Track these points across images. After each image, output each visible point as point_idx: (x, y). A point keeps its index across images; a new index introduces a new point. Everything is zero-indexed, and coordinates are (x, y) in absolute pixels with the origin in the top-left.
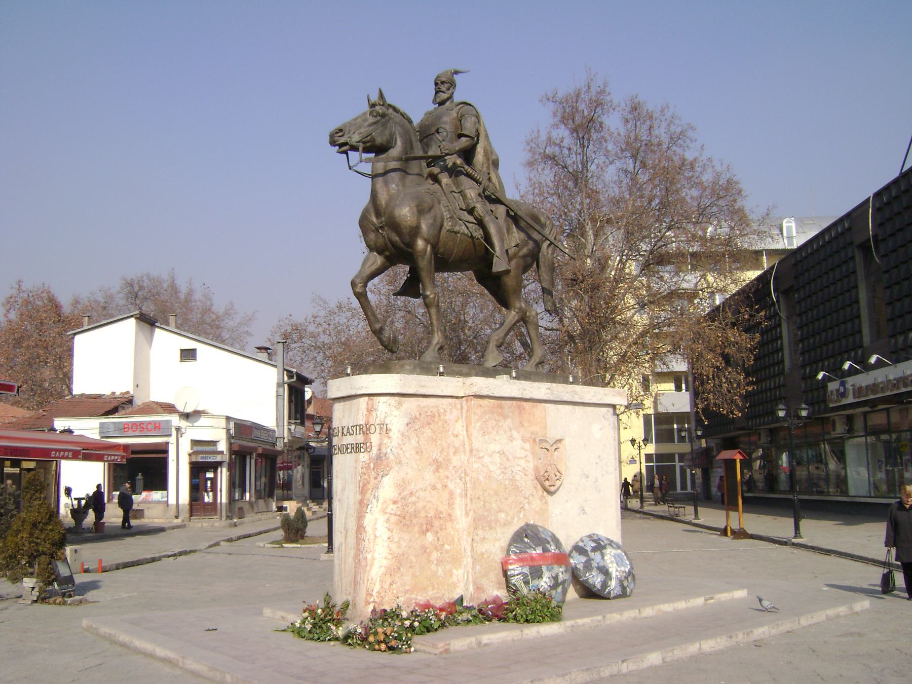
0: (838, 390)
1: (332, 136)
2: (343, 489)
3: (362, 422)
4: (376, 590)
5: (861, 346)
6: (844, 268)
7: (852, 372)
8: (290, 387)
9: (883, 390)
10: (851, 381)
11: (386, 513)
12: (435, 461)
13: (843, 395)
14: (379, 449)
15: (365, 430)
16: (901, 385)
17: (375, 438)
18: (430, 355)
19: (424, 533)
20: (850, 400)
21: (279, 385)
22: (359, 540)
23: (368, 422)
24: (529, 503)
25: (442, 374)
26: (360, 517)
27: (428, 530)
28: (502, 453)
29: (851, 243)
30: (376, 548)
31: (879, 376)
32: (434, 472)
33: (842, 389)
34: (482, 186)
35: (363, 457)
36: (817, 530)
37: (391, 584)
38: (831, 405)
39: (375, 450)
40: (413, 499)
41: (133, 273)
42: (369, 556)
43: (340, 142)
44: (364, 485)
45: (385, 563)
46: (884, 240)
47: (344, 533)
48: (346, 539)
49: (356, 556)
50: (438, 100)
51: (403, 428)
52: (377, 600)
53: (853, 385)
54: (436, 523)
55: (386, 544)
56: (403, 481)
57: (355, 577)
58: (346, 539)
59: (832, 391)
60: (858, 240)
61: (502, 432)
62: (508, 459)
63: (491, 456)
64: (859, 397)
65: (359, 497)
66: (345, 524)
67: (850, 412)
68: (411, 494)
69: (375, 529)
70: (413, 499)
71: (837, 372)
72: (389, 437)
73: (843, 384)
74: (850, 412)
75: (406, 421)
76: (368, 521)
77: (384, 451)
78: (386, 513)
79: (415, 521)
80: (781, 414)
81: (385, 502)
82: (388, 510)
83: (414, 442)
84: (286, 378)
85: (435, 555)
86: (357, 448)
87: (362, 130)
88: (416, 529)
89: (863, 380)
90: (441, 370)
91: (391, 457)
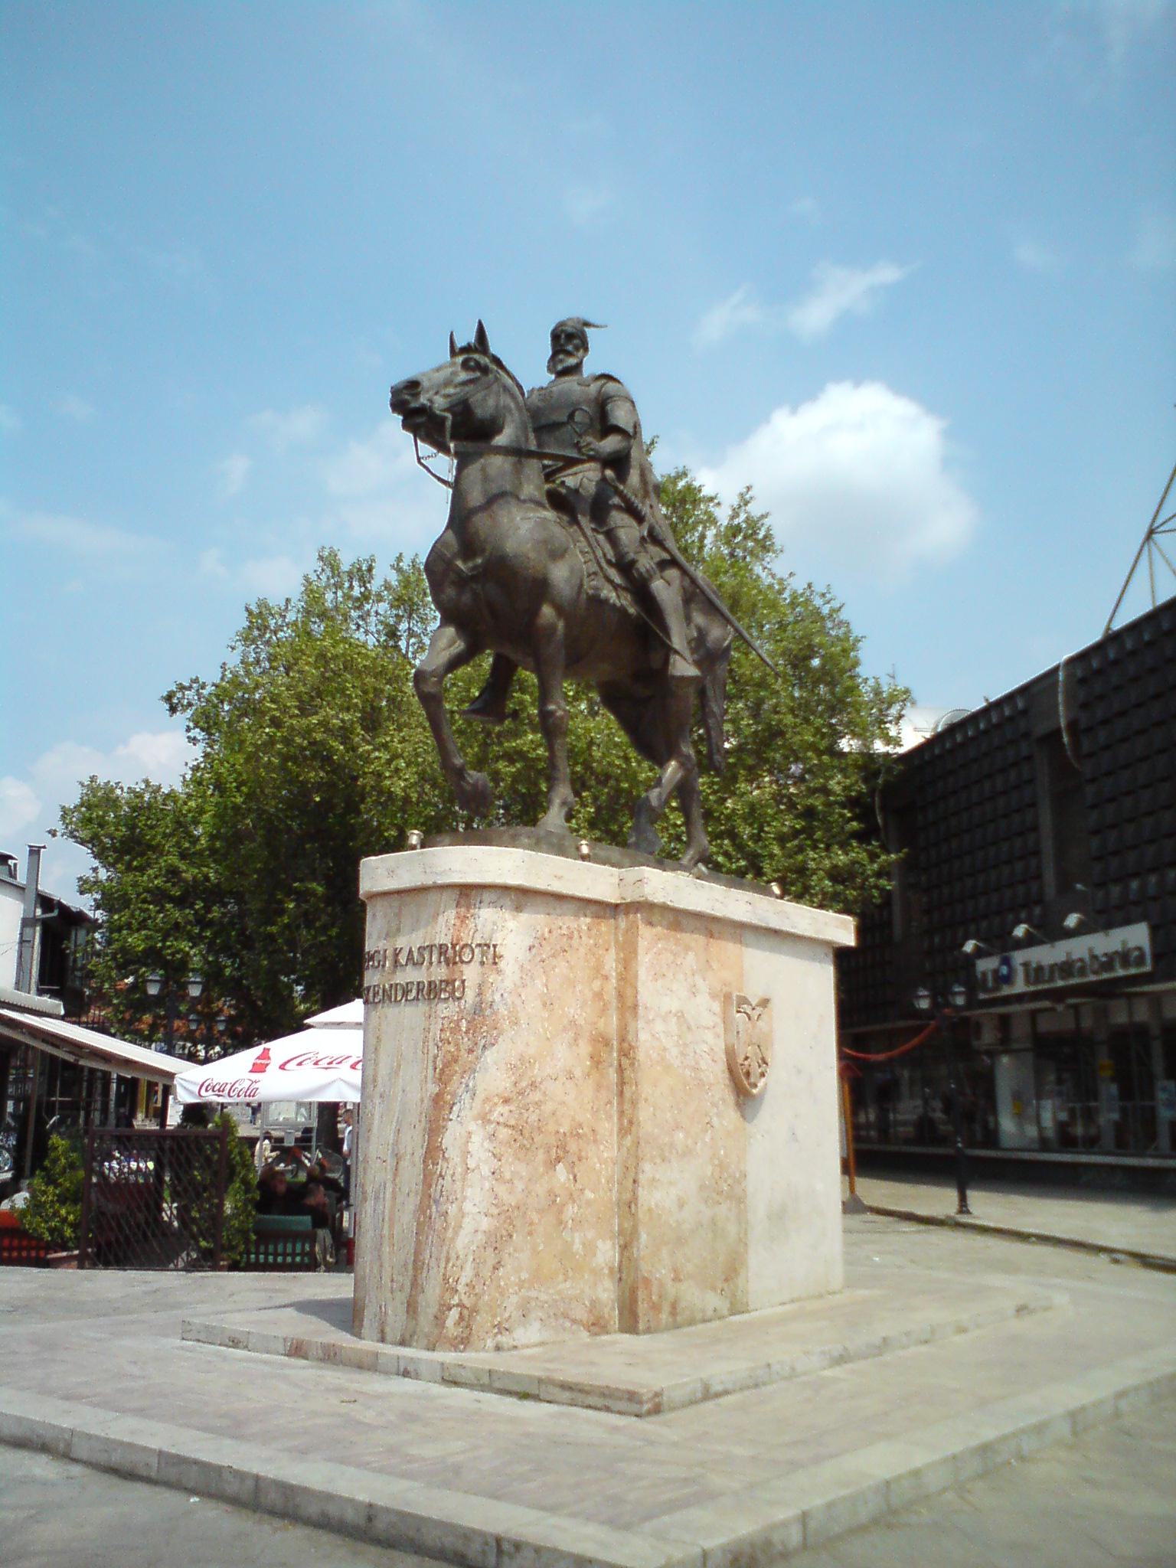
0: (996, 972)
1: (396, 392)
2: (395, 1072)
3: (443, 938)
4: (463, 1281)
5: (1040, 901)
6: (1013, 775)
7: (1029, 941)
8: (46, 924)
9: (1082, 971)
10: (1019, 957)
11: (489, 1121)
12: (573, 1023)
13: (1008, 979)
14: (479, 994)
15: (450, 955)
16: (1117, 965)
17: (471, 973)
18: (553, 818)
19: (552, 1164)
20: (1020, 986)
21: (27, 923)
22: (428, 1179)
23: (459, 939)
24: (718, 1115)
25: (584, 858)
26: (434, 1128)
27: (558, 1160)
28: (680, 1016)
29: (1026, 735)
30: (469, 1192)
31: (1078, 948)
32: (570, 1046)
33: (1004, 970)
34: (646, 526)
35: (446, 1010)
36: (989, 1206)
37: (495, 1268)
38: (982, 996)
39: (470, 995)
40: (536, 1096)
41: (632, 382)
42: (452, 1209)
43: (411, 408)
44: (447, 1065)
45: (485, 1224)
46: (1089, 730)
47: (391, 1162)
48: (395, 1175)
49: (423, 1209)
50: (560, 367)
51: (523, 955)
52: (466, 1302)
53: (1026, 965)
54: (573, 1146)
55: (487, 1185)
56: (521, 1059)
57: (417, 1253)
58: (395, 1175)
59: (984, 974)
60: (1041, 729)
61: (681, 977)
62: (689, 1028)
63: (665, 1020)
64: (1037, 981)
65: (433, 1089)
66: (396, 1143)
67: (1002, 1010)
68: (533, 1085)
69: (466, 1153)
70: (536, 1096)
71: (1001, 943)
72: (499, 972)
73: (1006, 961)
74: (1002, 1010)
75: (529, 942)
76: (450, 1139)
77: (488, 997)
78: (489, 1121)
79: (538, 1139)
80: (924, 1004)
81: (487, 1099)
82: (495, 1116)
83: (539, 983)
84: (39, 912)
85: (571, 1210)
86: (432, 992)
87: (451, 390)
88: (541, 1156)
89: (1047, 955)
90: (585, 850)
91: (503, 1011)
